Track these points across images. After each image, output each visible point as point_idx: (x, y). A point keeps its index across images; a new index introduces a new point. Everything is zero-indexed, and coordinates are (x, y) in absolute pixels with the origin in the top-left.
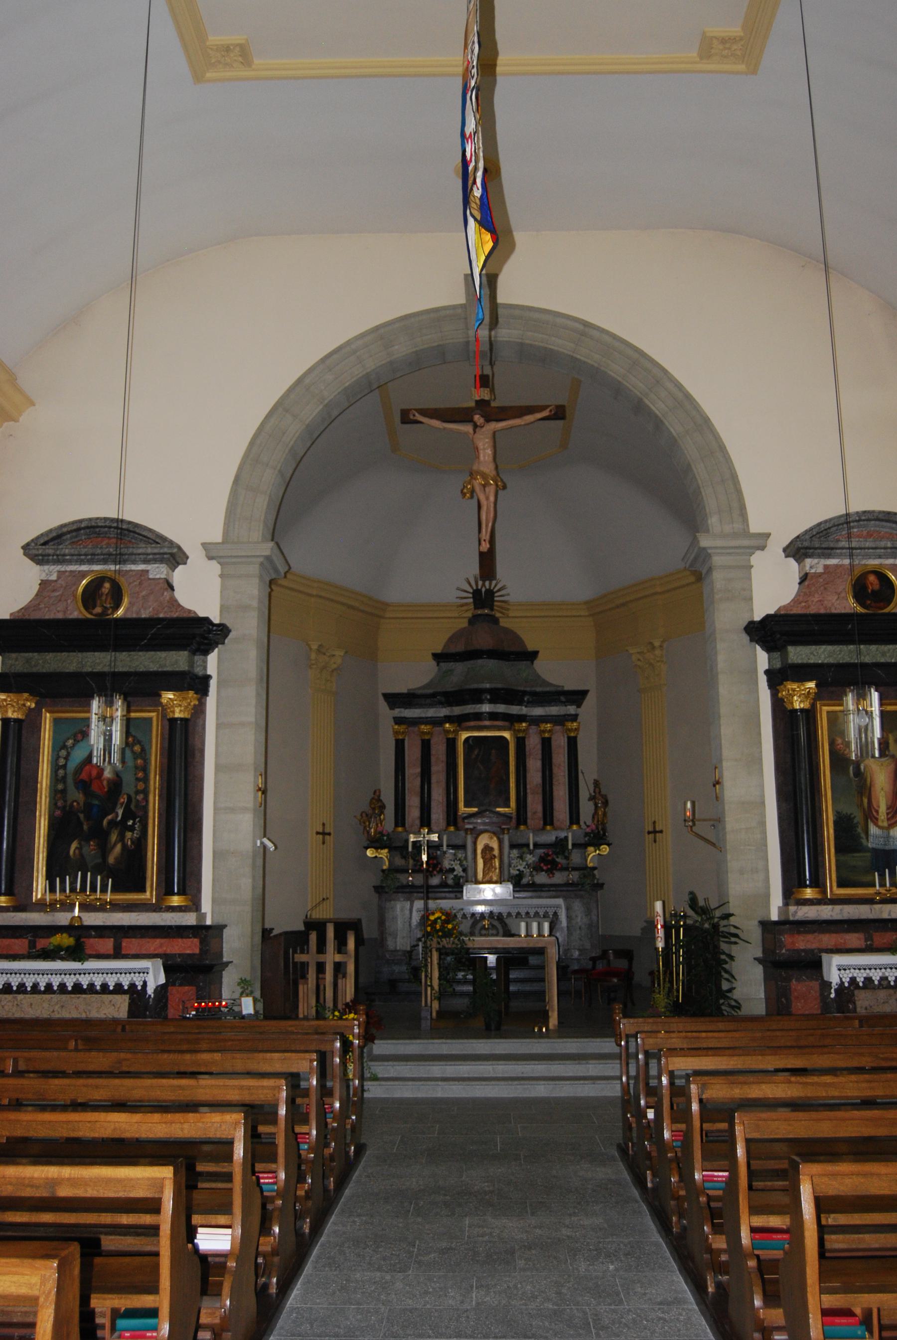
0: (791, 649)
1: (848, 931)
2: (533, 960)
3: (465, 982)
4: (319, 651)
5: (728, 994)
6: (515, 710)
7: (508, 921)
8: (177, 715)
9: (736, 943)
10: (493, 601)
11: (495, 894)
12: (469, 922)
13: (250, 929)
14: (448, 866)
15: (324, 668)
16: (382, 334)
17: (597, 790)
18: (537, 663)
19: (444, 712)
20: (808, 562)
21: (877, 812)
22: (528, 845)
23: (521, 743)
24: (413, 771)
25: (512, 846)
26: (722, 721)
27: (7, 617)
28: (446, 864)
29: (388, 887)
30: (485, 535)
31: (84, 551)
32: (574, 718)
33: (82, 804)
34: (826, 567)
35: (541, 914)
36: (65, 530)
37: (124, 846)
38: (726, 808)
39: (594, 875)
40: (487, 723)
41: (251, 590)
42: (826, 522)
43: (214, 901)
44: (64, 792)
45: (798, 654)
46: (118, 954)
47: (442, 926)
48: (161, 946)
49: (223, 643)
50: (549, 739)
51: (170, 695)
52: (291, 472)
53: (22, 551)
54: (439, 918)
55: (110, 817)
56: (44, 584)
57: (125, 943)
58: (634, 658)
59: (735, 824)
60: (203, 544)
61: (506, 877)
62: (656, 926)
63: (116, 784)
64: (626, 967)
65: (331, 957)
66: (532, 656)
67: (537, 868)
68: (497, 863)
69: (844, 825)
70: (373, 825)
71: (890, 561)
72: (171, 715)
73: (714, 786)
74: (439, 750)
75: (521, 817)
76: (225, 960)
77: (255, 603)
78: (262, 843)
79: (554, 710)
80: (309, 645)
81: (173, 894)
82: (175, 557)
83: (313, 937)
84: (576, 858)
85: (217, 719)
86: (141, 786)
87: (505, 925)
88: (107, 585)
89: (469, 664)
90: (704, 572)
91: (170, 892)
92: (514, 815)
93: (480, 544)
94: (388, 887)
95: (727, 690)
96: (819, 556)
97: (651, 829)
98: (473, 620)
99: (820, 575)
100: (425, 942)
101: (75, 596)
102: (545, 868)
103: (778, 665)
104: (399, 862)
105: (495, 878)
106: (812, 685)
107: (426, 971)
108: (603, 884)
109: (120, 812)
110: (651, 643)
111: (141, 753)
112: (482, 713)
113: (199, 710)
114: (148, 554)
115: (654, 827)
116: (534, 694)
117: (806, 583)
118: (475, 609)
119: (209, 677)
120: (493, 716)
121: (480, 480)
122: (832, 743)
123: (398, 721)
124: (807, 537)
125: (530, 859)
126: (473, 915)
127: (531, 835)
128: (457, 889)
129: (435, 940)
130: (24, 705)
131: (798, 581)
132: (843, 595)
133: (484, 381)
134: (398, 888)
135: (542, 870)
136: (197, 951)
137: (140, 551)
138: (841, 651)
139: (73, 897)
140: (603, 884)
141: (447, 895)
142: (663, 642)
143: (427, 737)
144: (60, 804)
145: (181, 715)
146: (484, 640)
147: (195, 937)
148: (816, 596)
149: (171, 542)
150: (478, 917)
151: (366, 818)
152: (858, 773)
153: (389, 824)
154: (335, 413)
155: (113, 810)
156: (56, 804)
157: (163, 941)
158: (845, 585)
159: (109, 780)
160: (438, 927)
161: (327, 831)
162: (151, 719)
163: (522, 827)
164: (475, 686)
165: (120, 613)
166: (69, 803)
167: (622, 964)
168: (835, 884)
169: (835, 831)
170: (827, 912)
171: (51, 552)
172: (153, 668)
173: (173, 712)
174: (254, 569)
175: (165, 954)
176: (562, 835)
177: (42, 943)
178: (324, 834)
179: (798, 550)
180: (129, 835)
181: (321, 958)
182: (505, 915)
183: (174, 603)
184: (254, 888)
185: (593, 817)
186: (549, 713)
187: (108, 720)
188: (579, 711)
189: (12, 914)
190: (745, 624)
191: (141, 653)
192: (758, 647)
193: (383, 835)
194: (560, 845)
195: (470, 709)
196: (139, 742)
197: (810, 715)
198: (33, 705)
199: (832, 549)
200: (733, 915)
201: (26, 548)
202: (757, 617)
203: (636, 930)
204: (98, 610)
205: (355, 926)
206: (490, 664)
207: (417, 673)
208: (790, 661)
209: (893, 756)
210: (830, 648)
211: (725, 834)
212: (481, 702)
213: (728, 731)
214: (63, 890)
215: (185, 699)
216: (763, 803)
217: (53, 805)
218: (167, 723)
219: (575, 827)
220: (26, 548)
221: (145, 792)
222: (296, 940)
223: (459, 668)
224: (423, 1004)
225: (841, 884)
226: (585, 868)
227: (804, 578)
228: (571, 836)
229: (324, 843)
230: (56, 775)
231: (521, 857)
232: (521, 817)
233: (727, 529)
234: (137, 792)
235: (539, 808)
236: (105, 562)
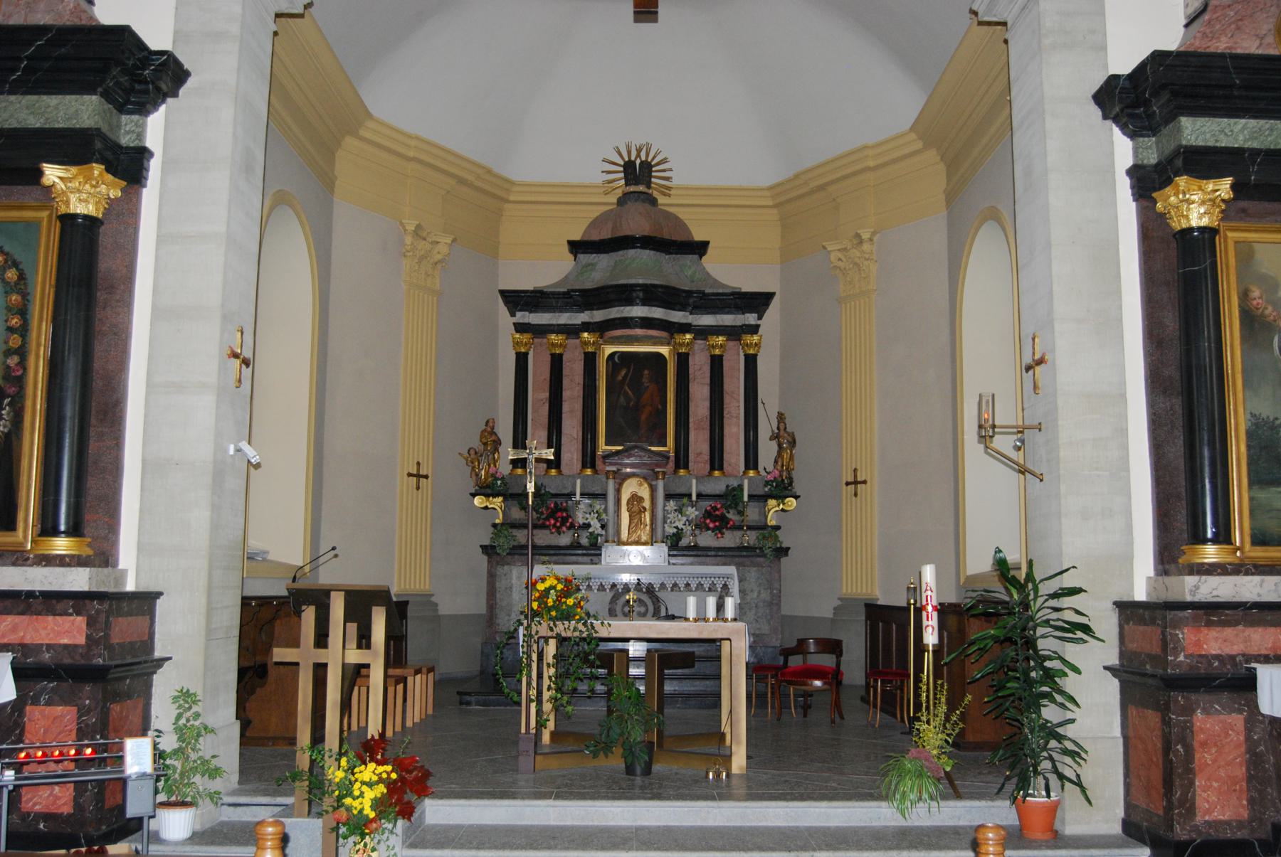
4: (418, 232)
5: (1060, 730)
6: (677, 316)
7: (661, 595)
10: (651, 177)
11: (644, 557)
12: (609, 595)
13: (204, 601)
14: (581, 521)
15: (421, 259)
17: (782, 426)
22: (690, 496)
23: (683, 360)
24: (537, 396)
25: (668, 497)
28: (580, 518)
35: (706, 586)
39: (777, 537)
40: (639, 332)
45: (1197, 131)
48: (14, 629)
54: (554, 588)
58: (833, 257)
61: (659, 535)
64: (834, 665)
65: (341, 652)
66: (700, 248)
67: (700, 526)
68: (647, 517)
75: (682, 460)
77: (235, 29)
78: (238, 450)
79: (728, 319)
80: (402, 224)
84: (752, 514)
85: (159, 227)
86: (15, 341)
87: (656, 601)
97: (851, 479)
98: (621, 202)
102: (711, 525)
104: (517, 514)
105: (644, 538)
108: (788, 549)
110: (858, 236)
111: (16, 284)
112: (632, 318)
113: (125, 212)
115: (855, 476)
116: (703, 295)
117: (1206, 17)
118: (627, 185)
120: (647, 323)
122: (1244, 295)
123: (520, 328)
125: (692, 512)
126: (614, 586)
127: (694, 481)
128: (593, 551)
129: (545, 624)
131: (1184, 22)
134: (514, 547)
135: (708, 529)
136: (81, 640)
138: (1272, 130)
140: (788, 549)
141: (580, 559)
142: (874, 234)
146: (636, 224)
147: (78, 614)
148: (1223, 39)
150: (620, 588)
151: (474, 457)
160: (550, 602)
163: (682, 472)
167: (827, 661)
169: (1249, 447)
172: (34, 122)
173: (67, 203)
175: (23, 646)
178: (418, 476)
181: (321, 656)
182: (657, 587)
184: (215, 527)
185: (776, 462)
186: (721, 323)
191: (12, 98)
192: (1116, 131)
193: (497, 479)
194: (732, 497)
195: (615, 313)
196: (15, 264)
202: (1123, 62)
206: (644, 257)
207: (551, 268)
208: (1184, 143)
210: (1252, 123)
212: (630, 302)
216: (1123, 396)
219: (751, 473)
224: (523, 730)
226: (764, 527)
229: (418, 488)
231: (680, 510)
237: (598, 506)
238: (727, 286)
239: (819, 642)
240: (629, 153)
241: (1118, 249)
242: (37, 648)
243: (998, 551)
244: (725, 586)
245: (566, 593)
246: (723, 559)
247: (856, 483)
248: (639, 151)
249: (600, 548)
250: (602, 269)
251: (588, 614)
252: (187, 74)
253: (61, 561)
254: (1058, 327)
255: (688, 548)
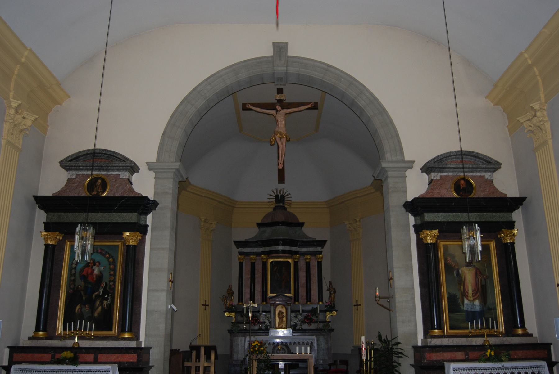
0: (425, 214)
1: (456, 351)
2: (301, 365)
3: (300, 350)
4: (206, 221)
6: (294, 249)
7: (290, 347)
8: (131, 243)
9: (401, 357)
11: (284, 334)
12: (272, 346)
13: (163, 349)
14: (262, 321)
16: (234, 68)
18: (304, 229)
19: (261, 250)
20: (433, 174)
21: (468, 293)
22: (299, 311)
23: (296, 264)
24: (247, 276)
25: (292, 312)
26: (393, 249)
27: (51, 195)
28: (262, 320)
29: (235, 330)
30: (281, 161)
31: (89, 165)
32: (320, 253)
33: (83, 286)
34: (441, 176)
35: (305, 343)
36: (80, 154)
37: (103, 308)
38: (396, 291)
40: (281, 255)
41: (170, 185)
42: (441, 155)
43: (146, 335)
44: (74, 281)
45: (429, 217)
46: (96, 362)
47: (259, 349)
48: (118, 357)
49: (155, 210)
50: (309, 262)
51: (127, 234)
52: (190, 131)
53: (59, 164)
54: (257, 344)
55: (96, 293)
56: (69, 180)
57: (100, 356)
59: (400, 299)
60: (147, 163)
62: (362, 349)
63: (100, 277)
65: (203, 363)
66: (302, 225)
67: (303, 322)
69: (452, 300)
70: (228, 301)
71: (471, 174)
72: (128, 244)
73: (389, 280)
74: (259, 267)
75: (296, 298)
76: (150, 365)
77: (171, 191)
78: (171, 307)
79: (311, 249)
81: (126, 332)
82: (133, 168)
83: (194, 353)
84: (321, 317)
86: (112, 278)
87: (288, 349)
88: (100, 181)
89: (274, 228)
90: (383, 180)
91: (124, 331)
92: (293, 297)
93: (278, 165)
94: (235, 330)
95: (395, 234)
96: (438, 172)
97: (355, 304)
98: (274, 209)
99: (438, 180)
100: (250, 356)
101: (84, 186)
103: (419, 222)
104: (240, 318)
105: (284, 326)
106: (436, 231)
107: (250, 371)
109: (101, 291)
110: (355, 220)
113: (142, 242)
114: (120, 167)
116: (303, 242)
117: (432, 184)
119: (147, 226)
120: (284, 252)
121: (278, 136)
122: (445, 260)
123: (241, 253)
124: (432, 162)
125: (300, 317)
126: (274, 343)
128: (266, 331)
129: (255, 355)
130: (56, 238)
132: (449, 190)
133: (280, 91)
134: (239, 330)
135: (306, 323)
136: (135, 360)
137: (116, 165)
138: (449, 215)
139: (75, 332)
143: (254, 261)
144: (72, 286)
145: (133, 244)
146: (280, 217)
149: (131, 161)
150: (276, 344)
151: (225, 298)
152: (458, 274)
153: (235, 301)
154: (212, 105)
155: (98, 290)
156: (70, 287)
157: (118, 355)
158: (450, 185)
159: (96, 275)
160: (256, 349)
161: (207, 304)
162: (118, 246)
163: (297, 303)
164: (275, 238)
165: (105, 194)
166: (76, 286)
167: (343, 367)
168: (448, 328)
169: (448, 302)
170: (445, 342)
171: (73, 164)
172: (120, 220)
173: (129, 242)
174: (171, 175)
175: (120, 362)
176: (315, 306)
177: (58, 356)
178: (205, 305)
179: (427, 169)
180: (105, 302)
181: (198, 364)
182: (288, 344)
183: (132, 190)
184: (166, 329)
187: (84, 238)
188: (322, 250)
189: (45, 341)
190: (404, 203)
192: (410, 214)
194: (314, 311)
196: (112, 257)
197: (435, 246)
198: (61, 238)
199: (444, 168)
200: (399, 343)
201: (61, 163)
202: (410, 199)
203: (348, 350)
204: (95, 193)
205: (214, 348)
206: (283, 228)
207: (250, 232)
209: (474, 266)
210: (444, 214)
211: (395, 304)
212: (278, 245)
213: (396, 254)
214: (70, 329)
215: (134, 236)
217: (69, 287)
218: (126, 247)
219: (321, 303)
220: (61, 163)
221: (114, 281)
222: (187, 356)
223: (269, 230)
225: (452, 328)
226: (326, 321)
227: (431, 182)
228: (319, 307)
230: (71, 273)
231: (296, 317)
232: (296, 298)
233: (394, 159)
234: (110, 281)
235: (305, 294)
236: (99, 170)
237: (268, 315)
238: (310, 238)
239: (341, 361)
240: (277, 192)
241: (410, 246)
242: (124, 363)
243: (379, 332)
244: (312, 343)
245: (261, 346)
246: (311, 333)
247: (357, 305)
248: (280, 191)
249: (268, 330)
250: (268, 232)
251: (267, 352)
252: (158, 204)
253: (128, 339)
254: (395, 270)
255: (299, 330)
